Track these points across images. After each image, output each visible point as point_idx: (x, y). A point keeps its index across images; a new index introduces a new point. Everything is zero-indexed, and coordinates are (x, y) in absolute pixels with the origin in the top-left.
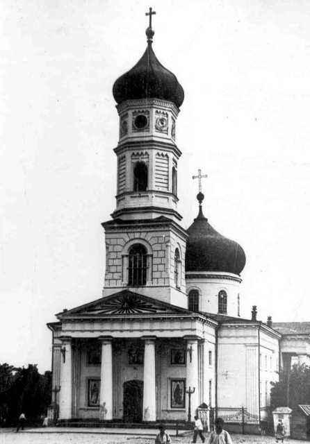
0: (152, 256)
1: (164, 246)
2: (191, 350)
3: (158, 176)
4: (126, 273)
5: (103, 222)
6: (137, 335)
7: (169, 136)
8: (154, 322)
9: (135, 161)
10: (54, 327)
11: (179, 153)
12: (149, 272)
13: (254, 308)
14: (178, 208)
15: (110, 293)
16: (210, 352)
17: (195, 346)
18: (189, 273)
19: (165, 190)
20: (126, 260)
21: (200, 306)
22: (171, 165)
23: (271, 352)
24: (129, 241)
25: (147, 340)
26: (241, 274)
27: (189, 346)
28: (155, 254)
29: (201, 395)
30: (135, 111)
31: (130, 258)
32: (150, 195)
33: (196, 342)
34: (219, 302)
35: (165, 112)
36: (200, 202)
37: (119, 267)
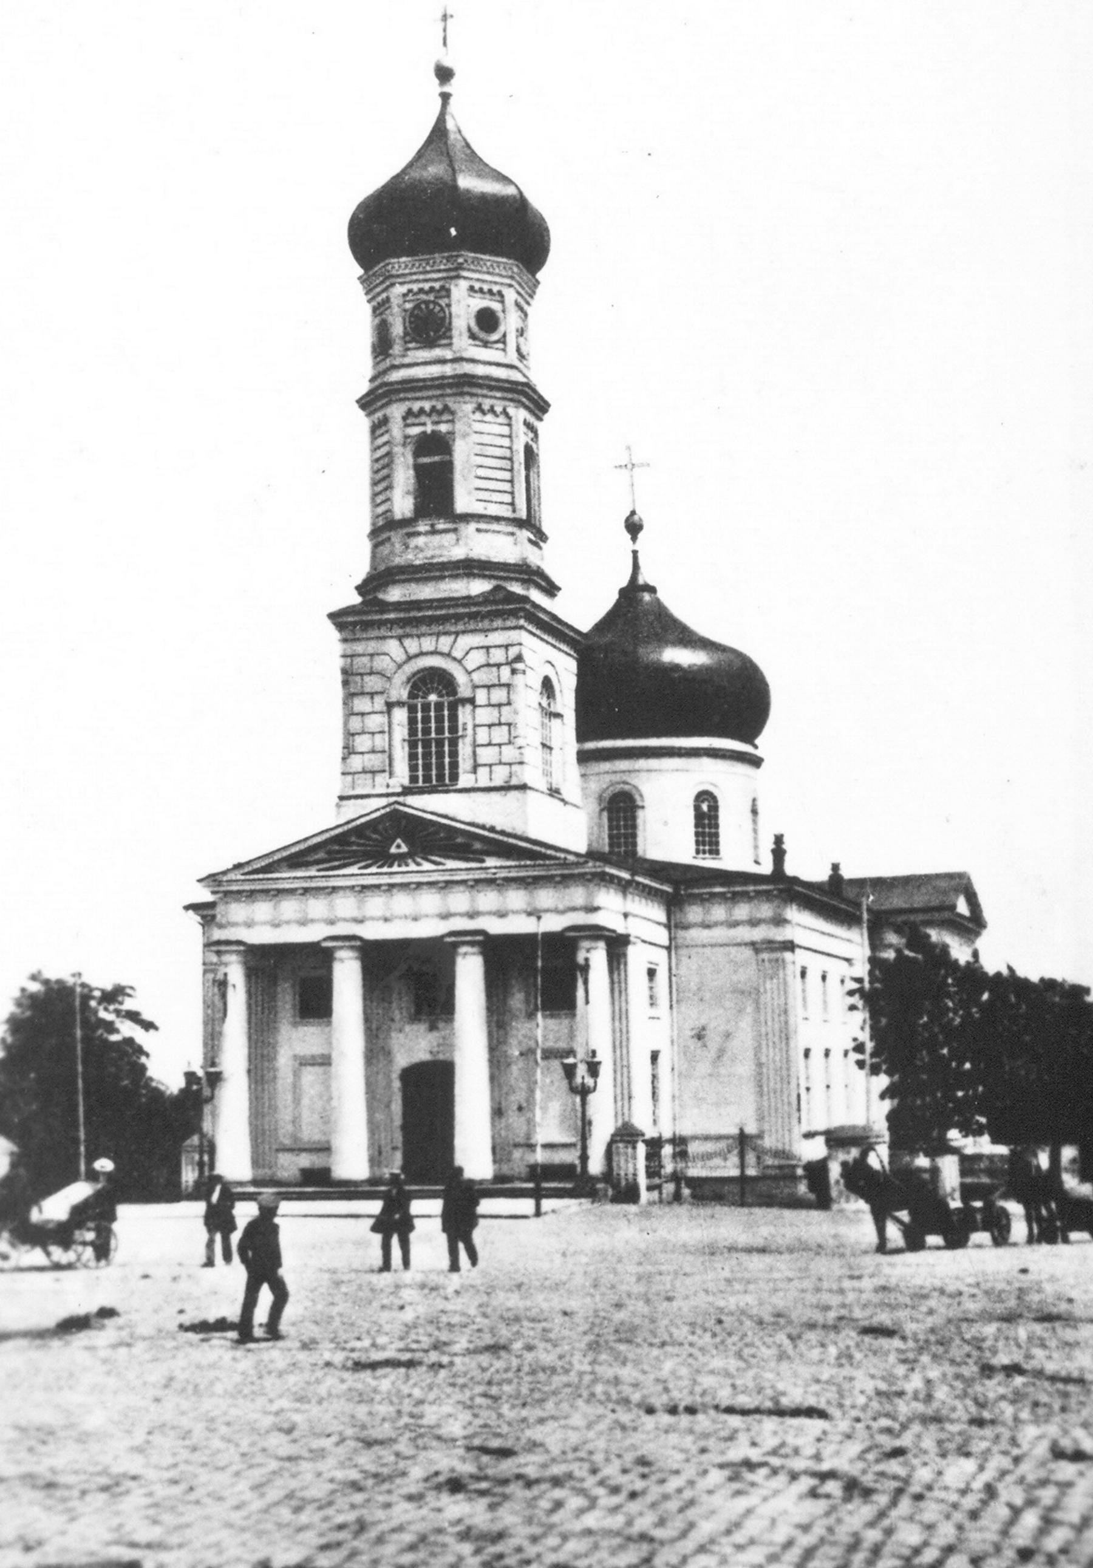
0: (472, 701)
1: (505, 671)
2: (585, 968)
3: (482, 472)
4: (401, 754)
5: (335, 607)
6: (553, 924)
7: (512, 357)
8: (418, 892)
9: (415, 431)
10: (205, 912)
11: (539, 406)
12: (464, 749)
13: (779, 840)
14: (547, 560)
15: (356, 811)
16: (651, 973)
17: (597, 957)
18: (591, 745)
19: (506, 512)
20: (400, 715)
21: (640, 840)
22: (522, 438)
23: (845, 964)
24: (432, 653)
25: (341, 948)
26: (757, 741)
27: (581, 957)
28: (481, 697)
29: (624, 1095)
30: (410, 291)
31: (412, 709)
32: (462, 526)
33: (601, 945)
34: (697, 826)
35: (495, 289)
36: (634, 538)
37: (378, 737)
